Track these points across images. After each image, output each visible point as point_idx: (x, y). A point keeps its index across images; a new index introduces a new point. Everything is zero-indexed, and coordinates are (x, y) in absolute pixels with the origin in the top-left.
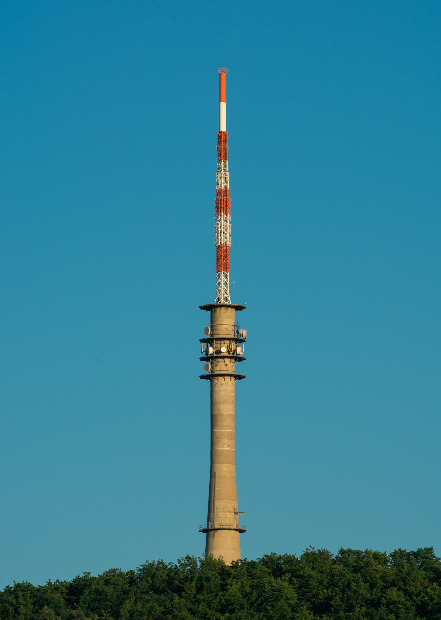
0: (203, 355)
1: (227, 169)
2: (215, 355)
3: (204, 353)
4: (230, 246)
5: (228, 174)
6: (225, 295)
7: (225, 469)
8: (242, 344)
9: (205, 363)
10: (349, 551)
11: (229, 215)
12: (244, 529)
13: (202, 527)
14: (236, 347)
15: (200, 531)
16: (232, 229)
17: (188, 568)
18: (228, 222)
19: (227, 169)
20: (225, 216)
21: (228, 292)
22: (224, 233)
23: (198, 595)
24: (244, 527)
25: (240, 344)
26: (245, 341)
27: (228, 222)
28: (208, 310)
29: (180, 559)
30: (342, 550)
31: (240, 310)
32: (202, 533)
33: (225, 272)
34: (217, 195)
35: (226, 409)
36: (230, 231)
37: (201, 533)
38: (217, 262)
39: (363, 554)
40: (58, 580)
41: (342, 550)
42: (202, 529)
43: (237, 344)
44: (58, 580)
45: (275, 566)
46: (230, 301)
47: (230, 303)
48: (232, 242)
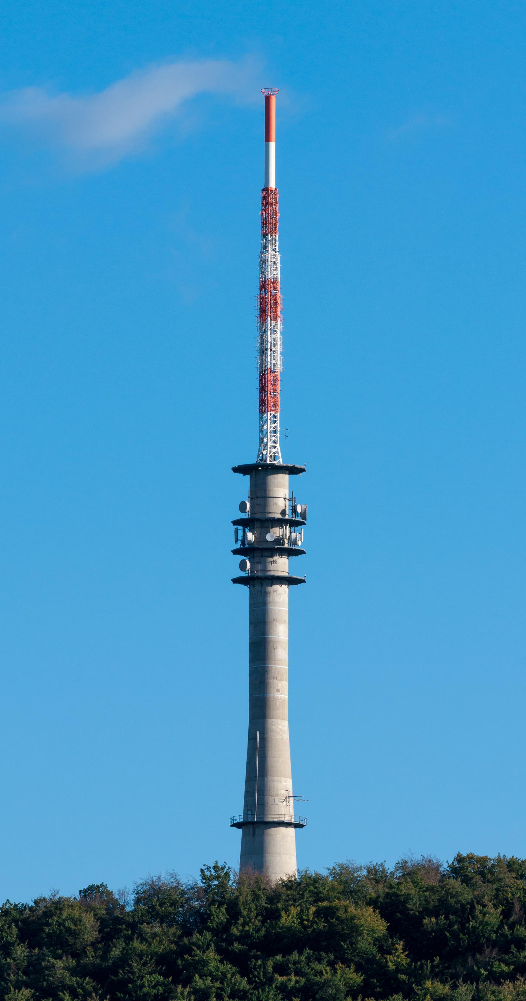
0: (238, 545)
1: (277, 248)
2: (256, 546)
3: (239, 542)
4: (282, 371)
5: (278, 256)
6: (275, 451)
7: (280, 728)
8: (300, 527)
9: (240, 558)
10: (471, 857)
11: (279, 322)
12: (301, 823)
13: (235, 818)
14: (291, 533)
15: (232, 826)
16: (284, 344)
17: (216, 883)
18: (279, 332)
19: (277, 248)
20: (273, 323)
21: (278, 445)
22: (271, 350)
23: (292, 907)
24: (301, 819)
25: (296, 528)
26: (303, 523)
27: (279, 332)
28: (245, 474)
29: (204, 868)
30: (459, 855)
31: (296, 473)
32: (235, 829)
33: (273, 413)
34: (261, 290)
35: (281, 633)
36: (282, 347)
37: (233, 828)
38: (261, 396)
39: (492, 862)
40: (8, 900)
41: (459, 855)
42: (235, 822)
43: (293, 529)
44: (8, 900)
45: (346, 883)
46: (281, 459)
47: (281, 463)
48: (284, 364)
